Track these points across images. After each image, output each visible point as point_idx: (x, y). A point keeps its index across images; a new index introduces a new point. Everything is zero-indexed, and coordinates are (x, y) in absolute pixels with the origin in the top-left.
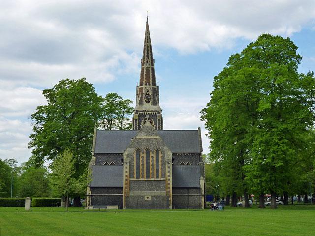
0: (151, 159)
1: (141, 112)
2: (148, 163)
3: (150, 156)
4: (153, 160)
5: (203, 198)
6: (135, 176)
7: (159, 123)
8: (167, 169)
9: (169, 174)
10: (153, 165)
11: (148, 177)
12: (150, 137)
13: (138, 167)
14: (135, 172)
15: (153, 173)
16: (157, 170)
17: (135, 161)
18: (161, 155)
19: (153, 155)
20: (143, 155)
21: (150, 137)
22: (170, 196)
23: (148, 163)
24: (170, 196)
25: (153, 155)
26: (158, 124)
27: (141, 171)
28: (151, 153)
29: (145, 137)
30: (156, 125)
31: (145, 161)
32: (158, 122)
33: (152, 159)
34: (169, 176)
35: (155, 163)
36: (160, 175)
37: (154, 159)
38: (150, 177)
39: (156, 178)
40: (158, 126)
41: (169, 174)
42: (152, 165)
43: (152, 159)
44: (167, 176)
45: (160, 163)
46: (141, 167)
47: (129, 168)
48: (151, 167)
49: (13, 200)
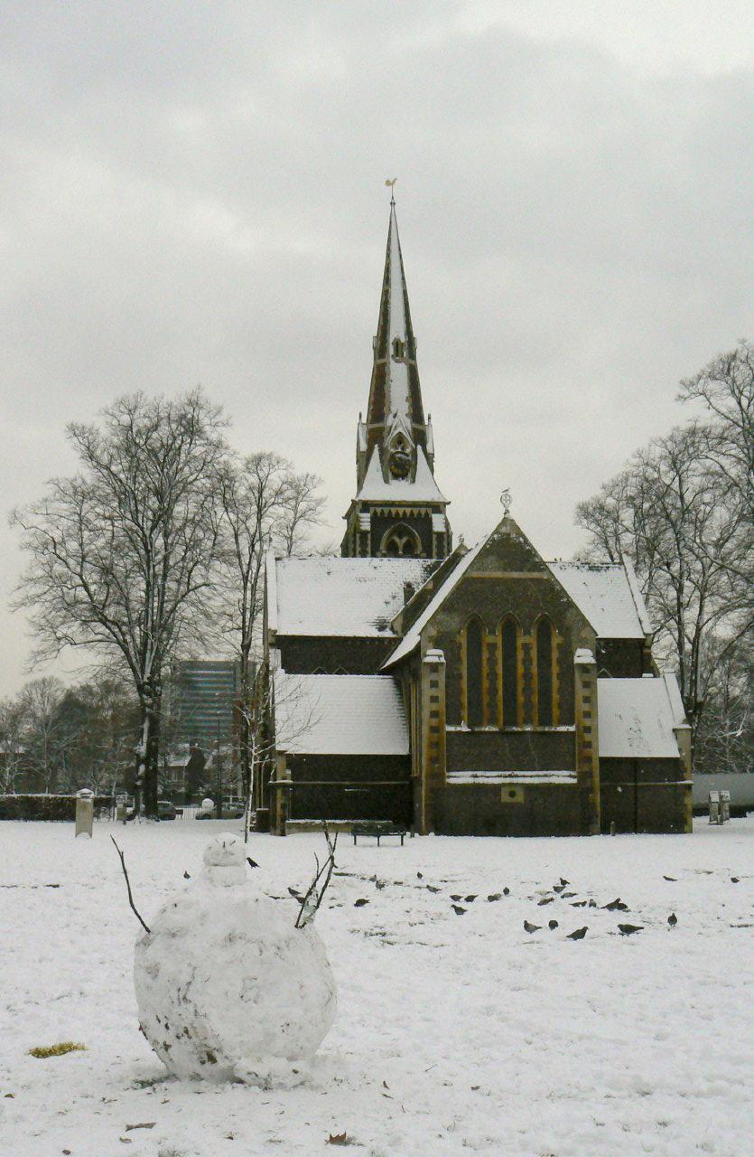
0: (520, 655)
1: (379, 510)
4: (527, 661)
6: (465, 713)
10: (527, 676)
11: (546, 719)
12: (516, 575)
14: (465, 700)
16: (545, 693)
18: (556, 640)
19: (527, 638)
20: (489, 639)
21: (516, 575)
24: (591, 790)
29: (499, 574)
32: (435, 543)
35: (535, 670)
36: (556, 712)
37: (534, 653)
38: (520, 720)
39: (542, 723)
42: (524, 675)
45: (555, 669)
46: (486, 684)
47: (442, 685)
48: (521, 684)
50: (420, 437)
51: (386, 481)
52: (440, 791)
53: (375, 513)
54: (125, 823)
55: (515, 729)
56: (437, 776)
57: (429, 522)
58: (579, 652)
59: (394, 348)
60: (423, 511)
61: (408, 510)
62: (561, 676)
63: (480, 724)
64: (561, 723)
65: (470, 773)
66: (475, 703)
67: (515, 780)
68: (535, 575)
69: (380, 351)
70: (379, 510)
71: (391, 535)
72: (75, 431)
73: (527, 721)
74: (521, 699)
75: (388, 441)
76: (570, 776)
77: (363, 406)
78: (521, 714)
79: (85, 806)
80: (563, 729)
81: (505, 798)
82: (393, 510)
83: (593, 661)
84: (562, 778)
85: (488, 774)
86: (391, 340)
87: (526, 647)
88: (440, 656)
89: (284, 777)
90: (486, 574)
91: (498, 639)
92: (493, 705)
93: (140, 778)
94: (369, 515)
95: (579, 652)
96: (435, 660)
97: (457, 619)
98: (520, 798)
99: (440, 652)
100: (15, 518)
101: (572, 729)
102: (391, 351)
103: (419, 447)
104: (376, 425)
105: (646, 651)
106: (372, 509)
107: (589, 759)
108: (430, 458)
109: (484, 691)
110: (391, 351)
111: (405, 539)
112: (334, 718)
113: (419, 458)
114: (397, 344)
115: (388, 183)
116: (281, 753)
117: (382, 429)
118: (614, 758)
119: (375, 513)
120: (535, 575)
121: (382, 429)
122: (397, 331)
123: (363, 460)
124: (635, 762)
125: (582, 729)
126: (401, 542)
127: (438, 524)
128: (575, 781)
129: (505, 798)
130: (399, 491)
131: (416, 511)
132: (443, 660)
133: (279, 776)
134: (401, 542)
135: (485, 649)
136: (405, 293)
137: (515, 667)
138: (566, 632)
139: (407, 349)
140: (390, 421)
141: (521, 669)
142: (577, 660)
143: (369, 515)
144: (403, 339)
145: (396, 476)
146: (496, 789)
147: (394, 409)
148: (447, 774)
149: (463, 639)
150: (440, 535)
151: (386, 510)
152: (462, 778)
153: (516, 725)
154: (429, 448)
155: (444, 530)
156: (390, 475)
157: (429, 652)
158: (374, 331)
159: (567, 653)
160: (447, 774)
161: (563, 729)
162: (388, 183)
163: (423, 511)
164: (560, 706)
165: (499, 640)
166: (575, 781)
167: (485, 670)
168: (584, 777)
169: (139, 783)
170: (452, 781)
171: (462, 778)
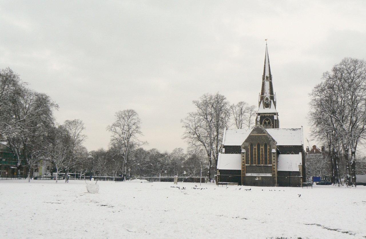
0: (261, 150)
1: (262, 115)
2: (259, 153)
3: (260, 148)
4: (262, 151)
5: (302, 179)
6: (250, 162)
7: (276, 123)
8: (273, 158)
9: (274, 161)
10: (262, 155)
11: (266, 163)
12: (260, 135)
13: (252, 156)
14: (250, 159)
15: (262, 160)
16: (266, 159)
17: (250, 152)
18: (268, 147)
19: (262, 147)
20: (254, 147)
21: (260, 135)
22: (275, 177)
23: (259, 153)
25: (262, 147)
26: (274, 124)
27: (254, 159)
28: (261, 146)
30: (274, 125)
31: (257, 152)
32: (274, 122)
33: (262, 150)
34: (274, 162)
35: (264, 153)
36: (268, 162)
37: (263, 150)
38: (261, 163)
39: (265, 164)
40: (275, 125)
41: (274, 161)
42: (262, 155)
43: (255, 151)
44: (272, 163)
45: (268, 153)
46: (254, 156)
47: (245, 156)
48: (261, 156)
49: (18, 157)
50: (272, 98)
51: (264, 108)
52: (245, 177)
53: (261, 115)
55: (260, 165)
56: (245, 174)
57: (273, 117)
58: (273, 150)
59: (268, 78)
60: (272, 115)
61: (269, 115)
63: (253, 164)
64: (269, 164)
65: (251, 174)
67: (259, 175)
68: (264, 134)
69: (264, 79)
71: (265, 120)
72: (194, 102)
73: (262, 163)
74: (261, 159)
75: (265, 99)
76: (271, 175)
77: (260, 92)
78: (261, 162)
79: (176, 179)
80: (269, 165)
82: (265, 115)
83: (276, 152)
84: (269, 175)
85: (254, 174)
86: (266, 76)
87: (262, 149)
88: (244, 151)
90: (254, 135)
91: (256, 147)
93: (208, 174)
94: (260, 116)
95: (273, 150)
96: (244, 152)
97: (248, 143)
98: (260, 179)
99: (245, 150)
100: (182, 121)
101: (271, 165)
102: (266, 79)
104: (262, 96)
105: (302, 148)
106: (260, 115)
107: (274, 171)
108: (275, 103)
109: (254, 158)
110: (266, 79)
111: (268, 121)
112: (228, 162)
113: (272, 104)
114: (267, 77)
115: (266, 40)
116: (218, 169)
117: (263, 97)
118: (286, 171)
119: (261, 115)
120: (264, 134)
121: (263, 97)
122: (267, 74)
123: (260, 103)
124: (290, 172)
126: (267, 122)
127: (275, 117)
128: (272, 176)
130: (267, 111)
131: (270, 115)
132: (245, 152)
133: (217, 174)
134: (267, 122)
135: (253, 149)
136: (269, 65)
137: (260, 153)
138: (270, 146)
139: (270, 78)
140: (265, 95)
141: (261, 153)
142: (272, 152)
143: (260, 116)
144: (268, 76)
145: (266, 107)
147: (266, 92)
148: (246, 174)
149: (249, 147)
150: (276, 120)
151: (264, 115)
152: (249, 175)
153: (260, 164)
154: (275, 100)
155: (277, 119)
156: (265, 107)
157: (242, 150)
158: (263, 74)
159: (270, 150)
160: (246, 174)
161: (269, 165)
162: (266, 40)
163: (272, 115)
164: (269, 161)
166: (272, 176)
167: (254, 153)
168: (274, 175)
169: (208, 175)
170: (247, 175)
171: (249, 175)
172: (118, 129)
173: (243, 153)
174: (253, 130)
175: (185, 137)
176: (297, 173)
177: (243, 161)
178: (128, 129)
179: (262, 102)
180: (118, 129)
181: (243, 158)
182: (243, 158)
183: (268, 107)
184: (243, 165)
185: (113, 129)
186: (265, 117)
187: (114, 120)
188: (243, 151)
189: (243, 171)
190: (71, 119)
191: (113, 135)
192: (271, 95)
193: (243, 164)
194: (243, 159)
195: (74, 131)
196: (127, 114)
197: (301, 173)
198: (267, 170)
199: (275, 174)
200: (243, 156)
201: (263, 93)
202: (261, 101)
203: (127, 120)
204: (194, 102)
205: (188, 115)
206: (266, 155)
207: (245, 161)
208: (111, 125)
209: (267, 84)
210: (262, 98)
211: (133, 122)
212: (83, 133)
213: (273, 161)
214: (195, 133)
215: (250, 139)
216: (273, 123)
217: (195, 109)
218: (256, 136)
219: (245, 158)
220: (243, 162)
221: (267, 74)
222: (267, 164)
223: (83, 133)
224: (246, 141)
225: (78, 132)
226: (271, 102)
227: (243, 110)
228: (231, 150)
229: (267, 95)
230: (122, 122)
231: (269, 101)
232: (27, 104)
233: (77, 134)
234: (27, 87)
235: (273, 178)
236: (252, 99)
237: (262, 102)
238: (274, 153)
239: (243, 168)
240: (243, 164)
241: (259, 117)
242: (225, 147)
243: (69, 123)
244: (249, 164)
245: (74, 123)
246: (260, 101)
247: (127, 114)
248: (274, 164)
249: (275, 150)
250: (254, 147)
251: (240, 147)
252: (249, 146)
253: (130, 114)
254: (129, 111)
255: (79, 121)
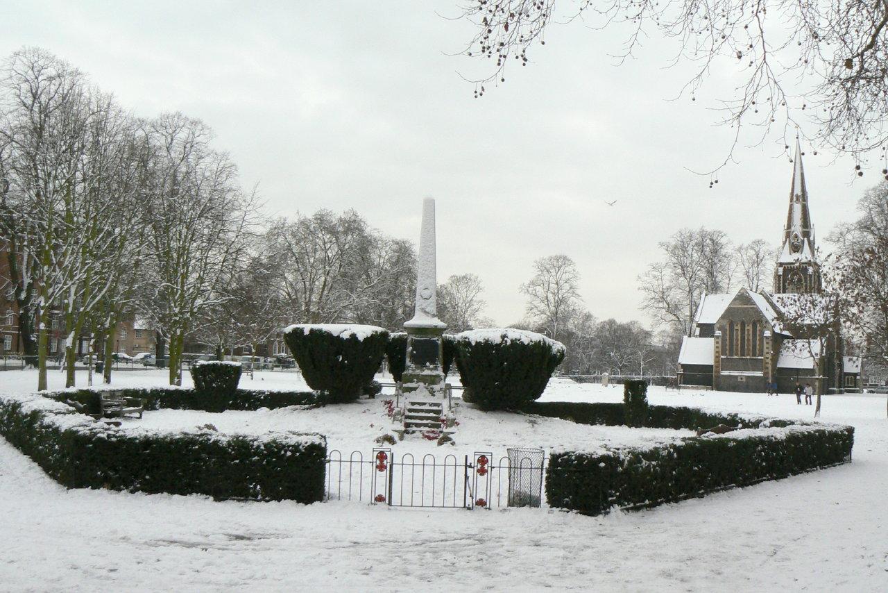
0: (746, 333)
1: (786, 266)
4: (749, 335)
6: (728, 352)
8: (765, 345)
11: (754, 354)
13: (731, 343)
14: (728, 348)
15: (749, 349)
16: (754, 346)
18: (758, 328)
19: (749, 328)
20: (736, 328)
23: (743, 339)
25: (749, 328)
36: (757, 352)
37: (751, 332)
41: (767, 351)
43: (737, 333)
44: (764, 354)
45: (758, 338)
46: (735, 343)
47: (720, 342)
50: (806, 235)
52: (719, 377)
54: (606, 386)
56: (719, 372)
60: (804, 265)
62: (759, 340)
66: (731, 350)
70: (786, 266)
72: (661, 244)
73: (748, 355)
74: (746, 347)
75: (792, 236)
81: (739, 380)
84: (759, 374)
87: (748, 330)
89: (681, 371)
92: (737, 349)
95: (766, 332)
102: (795, 199)
103: (806, 239)
110: (795, 199)
114: (797, 196)
116: (679, 364)
123: (784, 243)
124: (798, 370)
125: (40, 364)
129: (739, 380)
140: (793, 229)
144: (800, 194)
145: (795, 252)
146: (736, 377)
154: (811, 238)
159: (762, 333)
165: (739, 328)
172: (540, 290)
173: (718, 337)
174: (735, 299)
175: (647, 306)
176: (811, 372)
177: (717, 350)
178: (556, 291)
179: (788, 242)
180: (540, 290)
181: (717, 345)
182: (717, 345)
183: (798, 251)
184: (717, 357)
185: (530, 289)
186: (791, 270)
187: (531, 274)
188: (718, 333)
189: (717, 367)
190: (460, 274)
191: (530, 300)
192: (804, 230)
193: (717, 354)
194: (717, 347)
195: (464, 295)
196: (555, 263)
197: (817, 371)
198: (756, 365)
199: (768, 373)
200: (717, 343)
201: (789, 226)
202: (786, 240)
203: (554, 274)
204: (661, 244)
205: (650, 268)
206: (754, 341)
207: (720, 350)
208: (527, 282)
209: (798, 208)
210: (788, 235)
211: (565, 277)
212: (480, 296)
213: (765, 351)
214: (663, 299)
215: (729, 314)
216: (806, 281)
217: (663, 257)
218: (738, 309)
219: (720, 345)
220: (717, 352)
221: (798, 191)
222: (755, 356)
223: (480, 296)
224: (723, 317)
225: (472, 295)
226: (803, 241)
227: (761, 255)
228: (706, 330)
229: (797, 229)
230: (546, 276)
231: (799, 241)
232: (381, 257)
233: (469, 299)
234: (376, 234)
235: (765, 378)
236: (775, 238)
237: (788, 242)
238: (767, 338)
239: (716, 362)
240: (717, 354)
241: (781, 269)
242: (699, 325)
243: (457, 280)
244: (726, 355)
245: (465, 280)
246: (784, 240)
247: (555, 263)
248: (767, 356)
249: (769, 332)
250: (736, 328)
251: (711, 325)
252: (728, 326)
253: (561, 262)
254: (558, 259)
255: (472, 278)
